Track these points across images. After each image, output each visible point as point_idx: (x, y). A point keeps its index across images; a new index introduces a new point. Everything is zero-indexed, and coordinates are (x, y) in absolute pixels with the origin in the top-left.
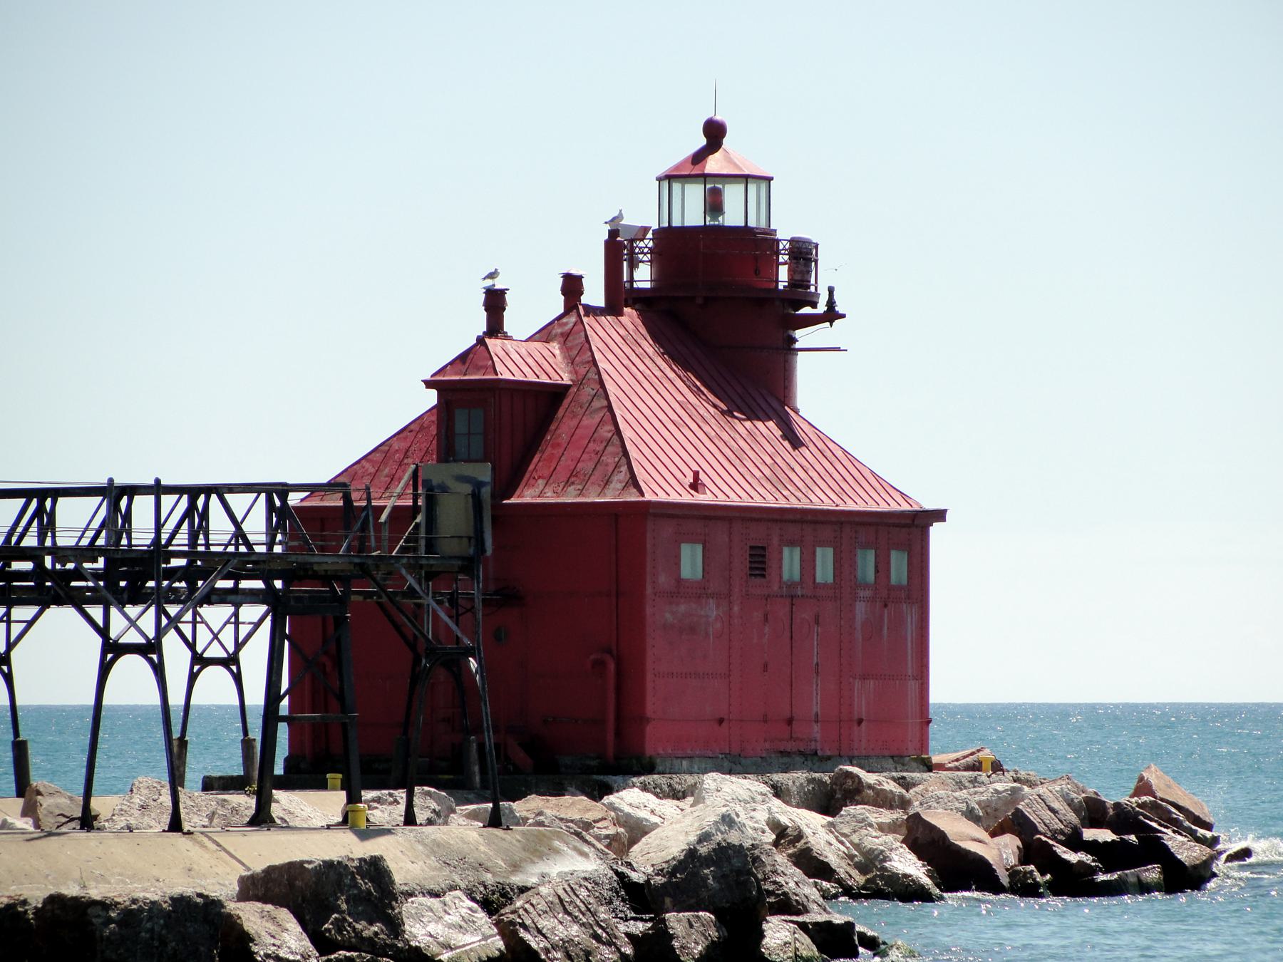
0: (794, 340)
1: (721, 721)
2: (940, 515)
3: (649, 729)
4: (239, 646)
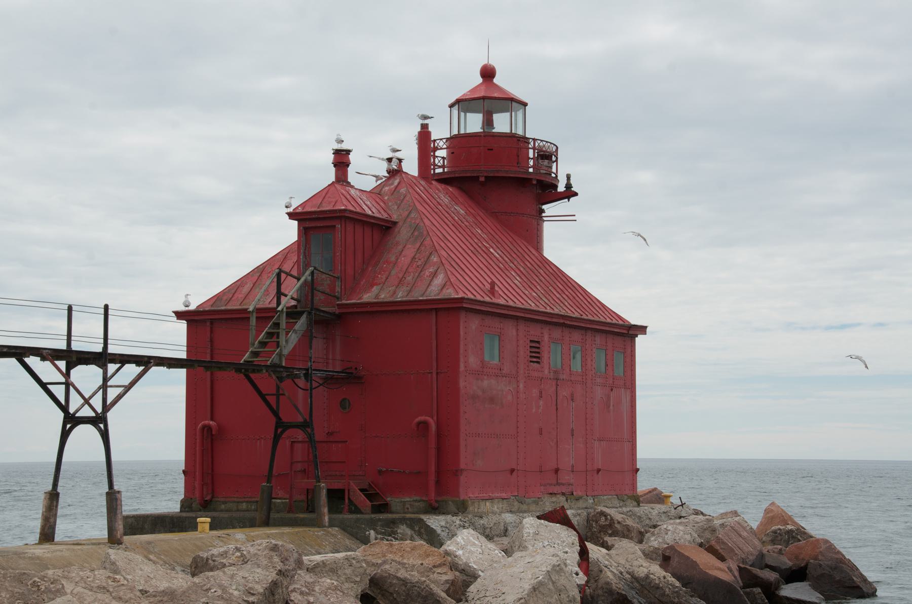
0: (543, 211)
1: (512, 471)
2: (642, 329)
3: (463, 479)
4: (106, 408)
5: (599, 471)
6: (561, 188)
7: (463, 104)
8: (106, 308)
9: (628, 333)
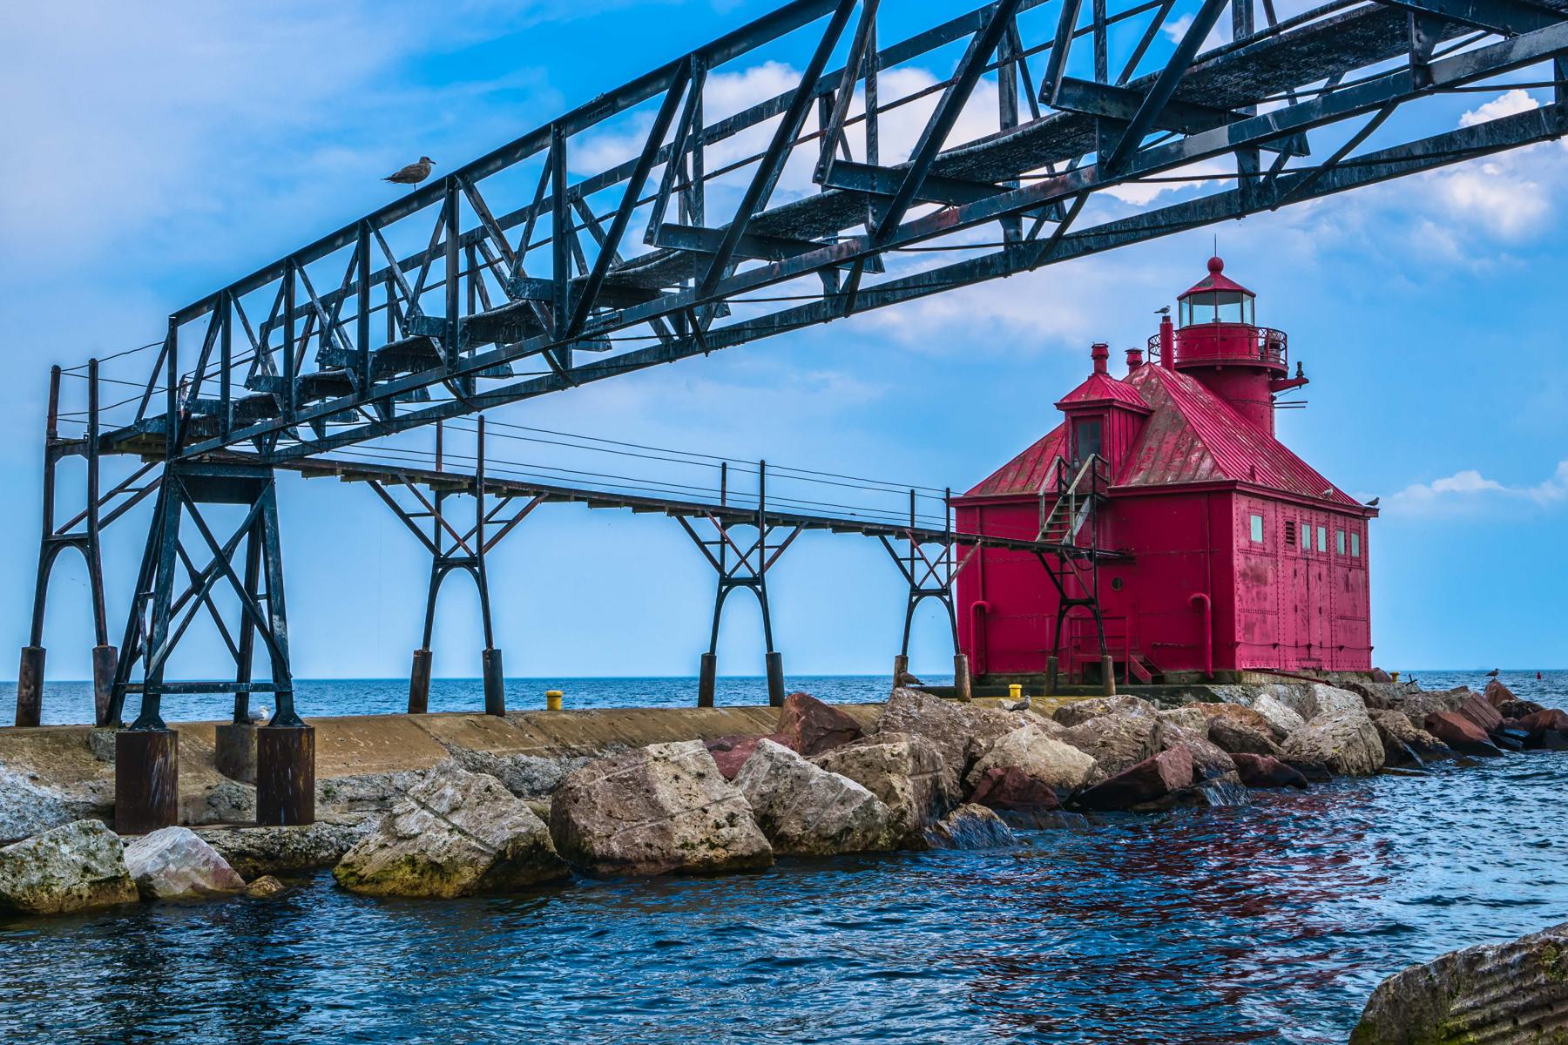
4: (763, 568)
5: (1341, 648)
6: (1292, 375)
7: (1195, 296)
8: (763, 464)
9: (1356, 516)
